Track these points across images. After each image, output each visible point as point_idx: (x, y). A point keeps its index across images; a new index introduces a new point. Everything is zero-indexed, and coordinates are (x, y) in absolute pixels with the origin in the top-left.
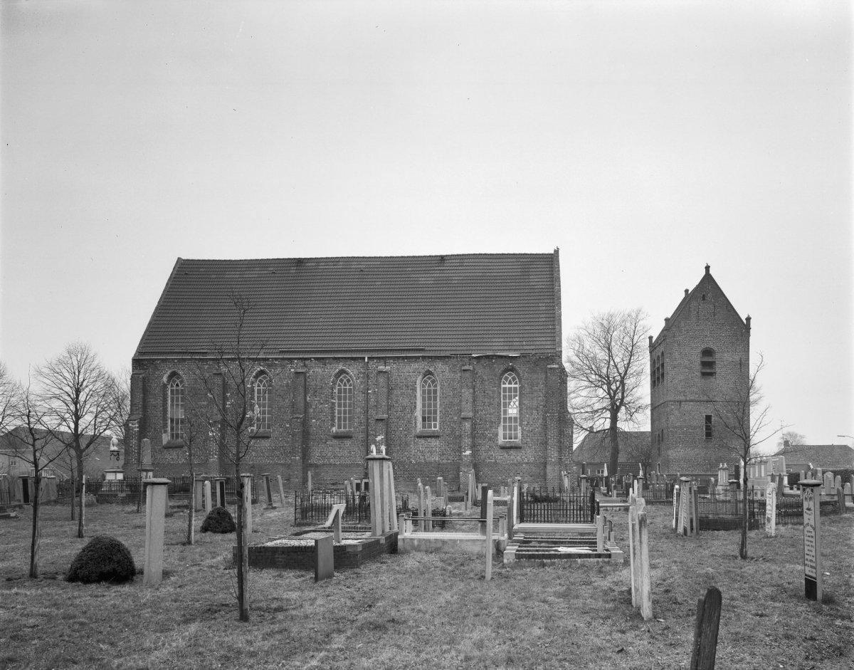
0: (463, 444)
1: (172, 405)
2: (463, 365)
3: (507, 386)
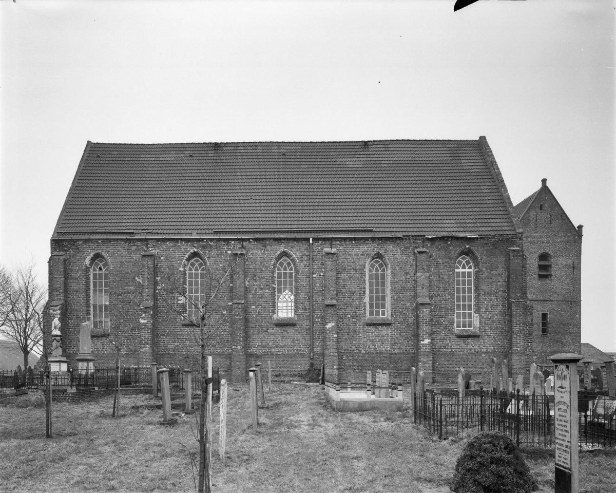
0: (421, 332)
1: (95, 291)
2: (416, 247)
3: (461, 270)
